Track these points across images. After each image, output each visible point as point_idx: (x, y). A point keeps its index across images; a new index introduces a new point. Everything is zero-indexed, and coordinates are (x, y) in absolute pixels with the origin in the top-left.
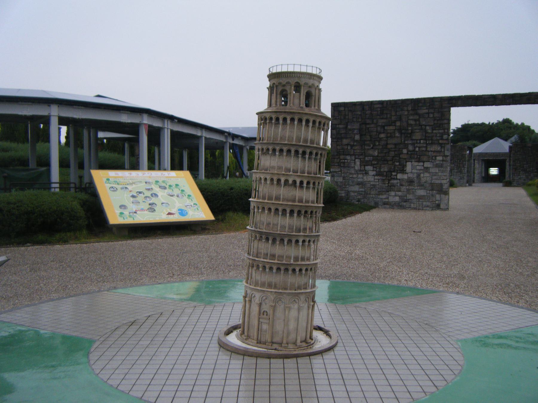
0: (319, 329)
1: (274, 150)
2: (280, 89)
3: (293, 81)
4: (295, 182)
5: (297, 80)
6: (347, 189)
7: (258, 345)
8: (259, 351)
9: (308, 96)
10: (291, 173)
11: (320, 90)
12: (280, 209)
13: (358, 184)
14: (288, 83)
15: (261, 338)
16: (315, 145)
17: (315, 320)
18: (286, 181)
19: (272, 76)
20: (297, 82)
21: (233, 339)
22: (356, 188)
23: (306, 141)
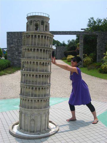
0: (50, 122)
1: (34, 49)
2: (35, 23)
3: (41, 20)
4: (43, 63)
5: (42, 20)
6: (13, 62)
7: (30, 133)
8: (34, 136)
9: (46, 26)
10: (42, 59)
11: (49, 24)
12: (38, 75)
13: (17, 60)
14: (38, 20)
15: (31, 129)
16: (48, 47)
17: (49, 118)
18: (40, 63)
19: (28, 18)
20: (42, 21)
21: (15, 130)
22: (16, 61)
23: (42, 45)
